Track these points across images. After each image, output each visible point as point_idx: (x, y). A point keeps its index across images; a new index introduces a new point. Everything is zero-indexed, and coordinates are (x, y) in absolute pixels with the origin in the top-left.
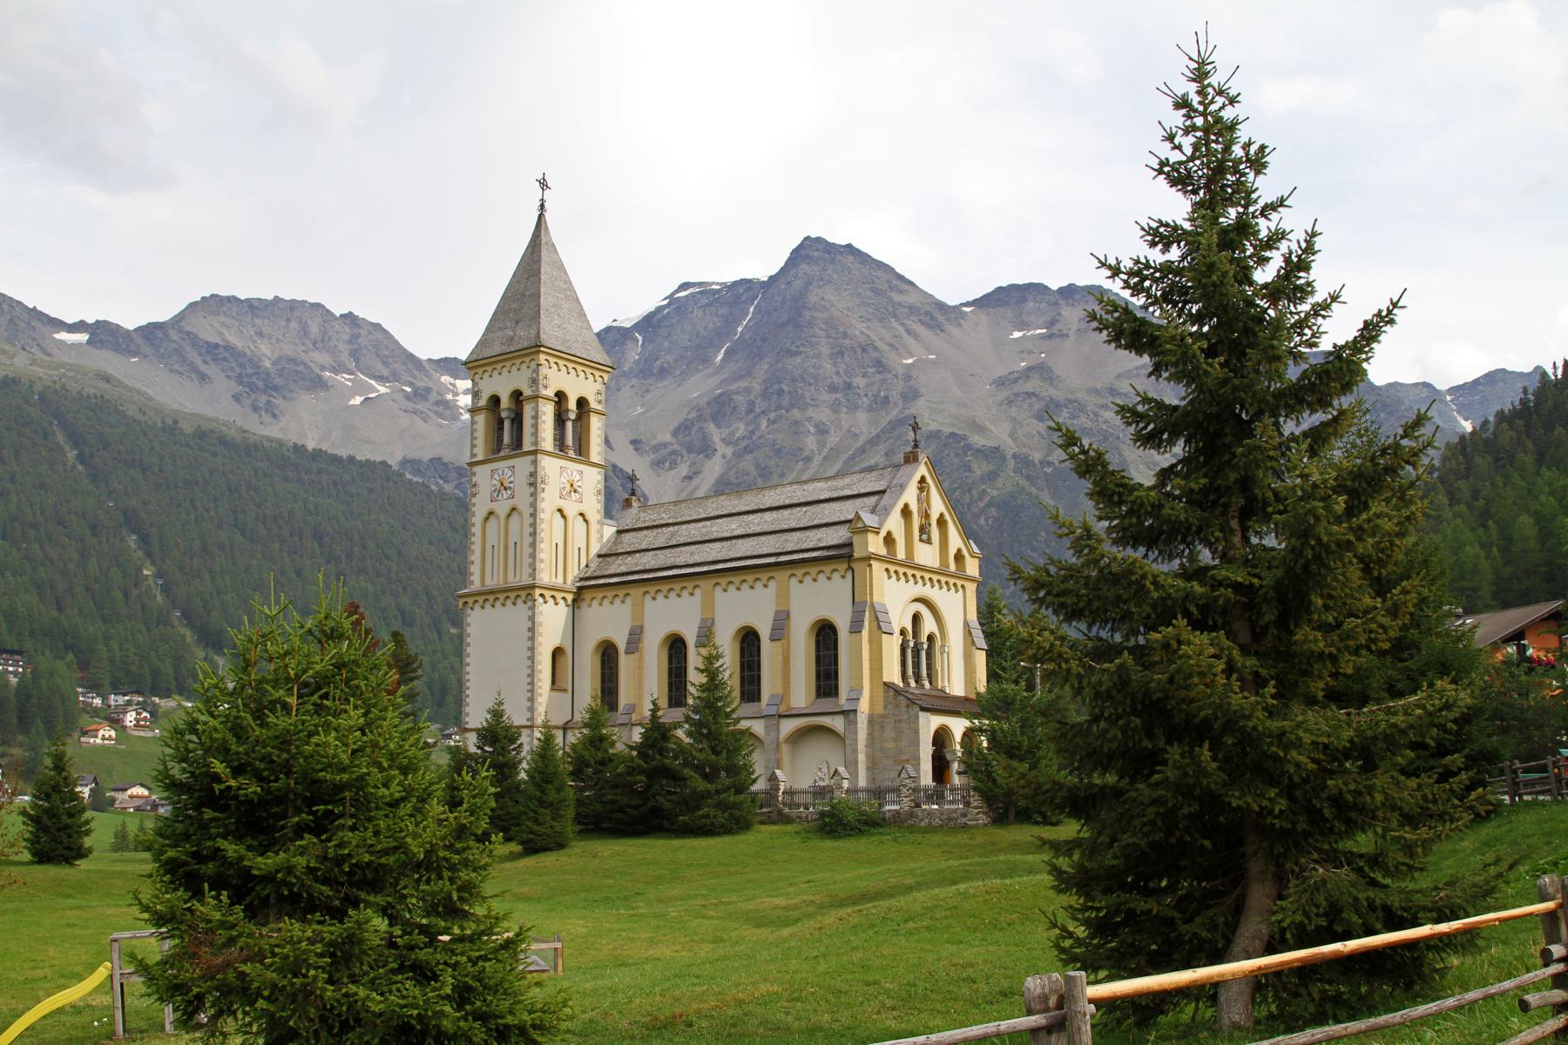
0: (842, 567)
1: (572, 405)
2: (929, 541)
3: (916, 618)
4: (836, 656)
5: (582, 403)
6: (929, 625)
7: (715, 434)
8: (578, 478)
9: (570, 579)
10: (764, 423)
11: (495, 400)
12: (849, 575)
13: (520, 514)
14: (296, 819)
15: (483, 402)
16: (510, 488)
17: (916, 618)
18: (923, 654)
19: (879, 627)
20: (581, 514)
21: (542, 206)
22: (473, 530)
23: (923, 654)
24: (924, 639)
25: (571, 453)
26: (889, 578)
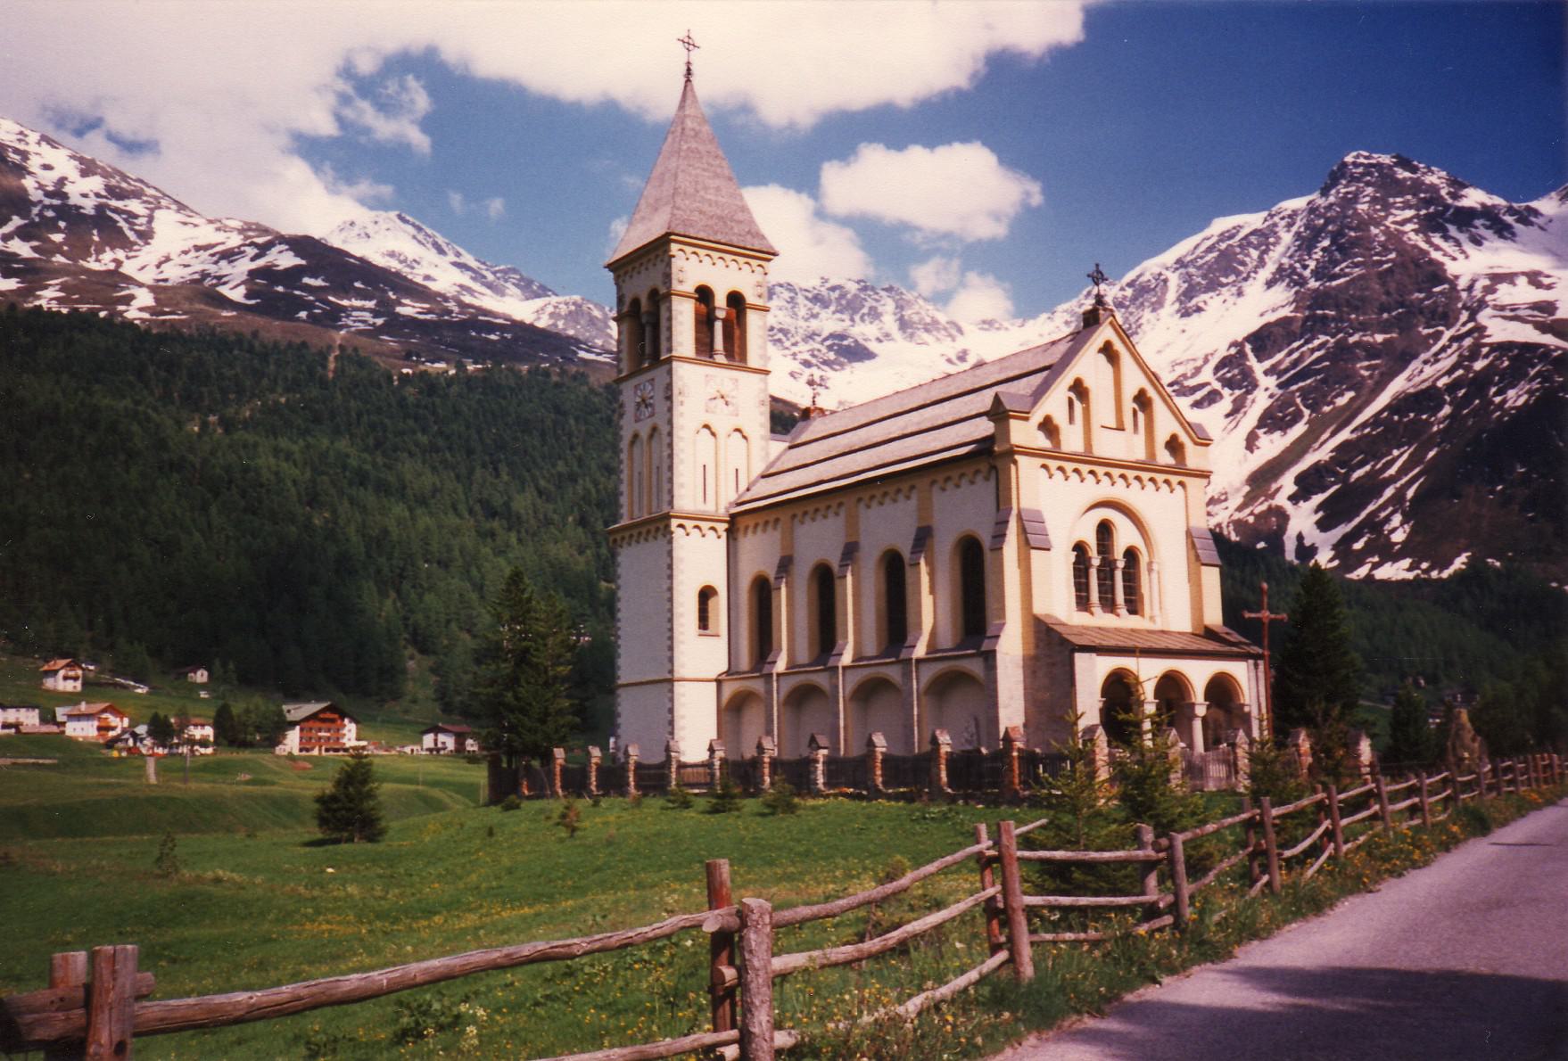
0: (984, 467)
1: (720, 301)
3: (1105, 530)
5: (736, 300)
6: (1125, 535)
7: (1258, 368)
11: (636, 302)
16: (651, 405)
17: (1105, 530)
18: (1119, 575)
19: (1027, 542)
20: (738, 430)
21: (689, 70)
23: (1119, 575)
25: (721, 359)
26: (1098, 482)
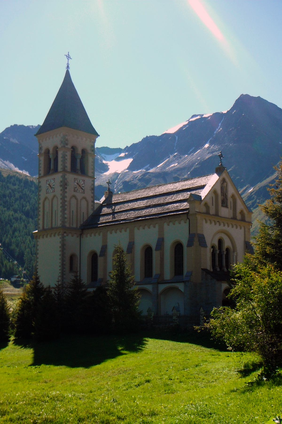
2: (226, 207)
4: (182, 257)
8: (82, 183)
9: (79, 225)
10: (254, 284)
12: (188, 220)
13: (57, 198)
14: (20, 330)
15: (43, 152)
16: (53, 188)
21: (68, 67)
22: (61, 218)
24: (224, 249)
